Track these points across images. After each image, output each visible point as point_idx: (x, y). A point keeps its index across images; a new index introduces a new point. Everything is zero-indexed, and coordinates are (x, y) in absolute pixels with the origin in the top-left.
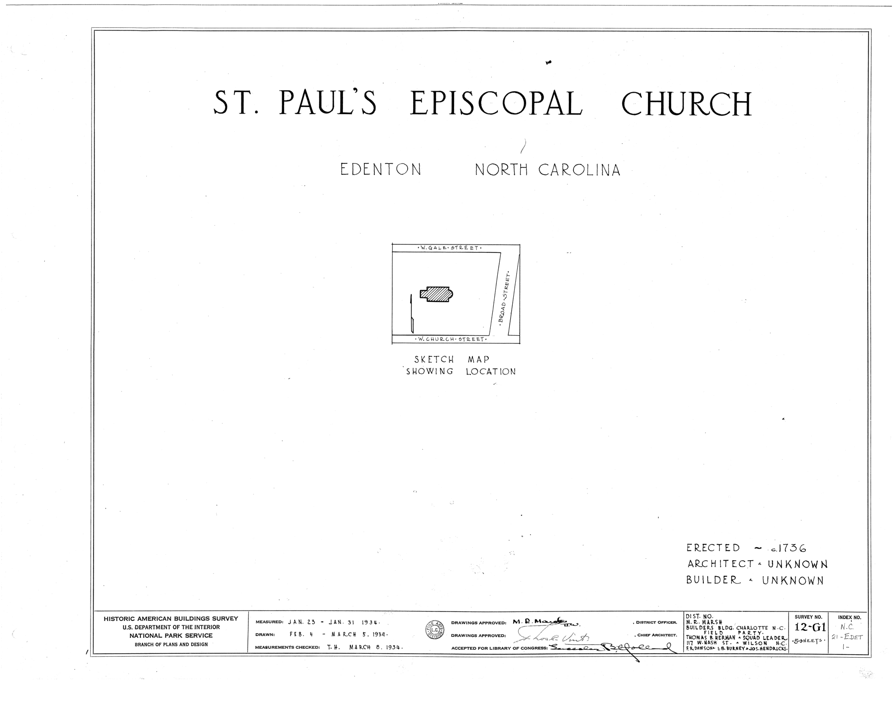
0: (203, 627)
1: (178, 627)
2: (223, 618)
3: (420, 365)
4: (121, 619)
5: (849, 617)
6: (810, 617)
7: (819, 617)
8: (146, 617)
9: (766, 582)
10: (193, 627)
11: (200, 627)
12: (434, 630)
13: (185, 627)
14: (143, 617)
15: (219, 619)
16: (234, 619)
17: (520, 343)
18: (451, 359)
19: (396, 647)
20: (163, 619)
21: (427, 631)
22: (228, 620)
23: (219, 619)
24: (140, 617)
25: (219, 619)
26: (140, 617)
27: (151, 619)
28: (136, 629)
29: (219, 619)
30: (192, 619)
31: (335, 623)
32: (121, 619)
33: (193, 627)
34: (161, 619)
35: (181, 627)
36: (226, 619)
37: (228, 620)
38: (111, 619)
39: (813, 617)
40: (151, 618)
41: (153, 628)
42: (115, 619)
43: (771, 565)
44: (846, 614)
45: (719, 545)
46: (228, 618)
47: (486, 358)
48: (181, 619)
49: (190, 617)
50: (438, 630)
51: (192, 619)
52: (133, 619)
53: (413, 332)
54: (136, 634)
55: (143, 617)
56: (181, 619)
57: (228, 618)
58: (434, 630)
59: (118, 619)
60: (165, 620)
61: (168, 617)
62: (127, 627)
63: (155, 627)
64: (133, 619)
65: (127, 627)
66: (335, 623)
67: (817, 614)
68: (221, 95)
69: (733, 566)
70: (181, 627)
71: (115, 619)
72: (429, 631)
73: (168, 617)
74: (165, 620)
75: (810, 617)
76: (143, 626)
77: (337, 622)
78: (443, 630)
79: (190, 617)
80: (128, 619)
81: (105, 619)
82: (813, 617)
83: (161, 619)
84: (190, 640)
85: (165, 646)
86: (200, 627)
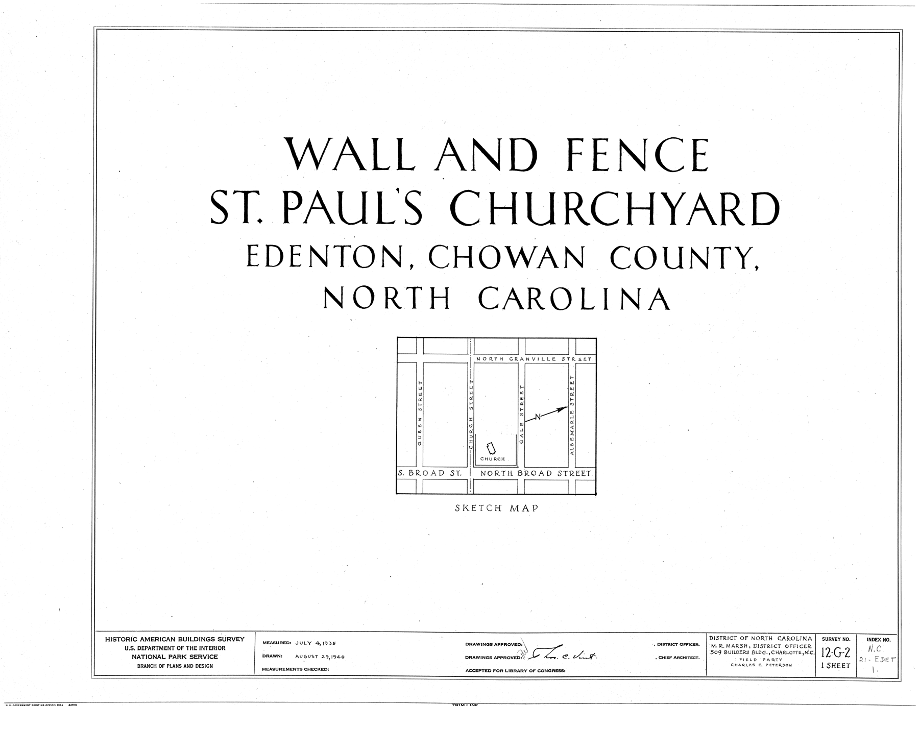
0: (208, 648)
1: (182, 648)
5: (878, 640)
6: (838, 639)
7: (847, 639)
8: (149, 638)
13: (189, 648)
14: (146, 638)
15: (224, 640)
16: (240, 639)
20: (166, 639)
22: (234, 641)
23: (224, 640)
24: (142, 638)
25: (224, 640)
26: (142, 638)
27: (154, 640)
28: (138, 650)
29: (224, 640)
30: (196, 639)
33: (198, 648)
34: (164, 639)
35: (185, 648)
36: (232, 640)
37: (234, 641)
38: (112, 640)
39: (841, 639)
40: (154, 639)
41: (156, 648)
42: (117, 639)
46: (234, 638)
48: (185, 639)
49: (195, 638)
52: (135, 639)
55: (146, 638)
56: (185, 639)
57: (234, 638)
59: (120, 639)
61: (172, 638)
63: (158, 648)
64: (135, 639)
67: (886, 637)
70: (185, 648)
71: (117, 639)
73: (172, 638)
75: (838, 639)
76: (146, 647)
79: (195, 638)
80: (130, 640)
81: (106, 639)
82: (841, 639)
83: (164, 639)
85: (169, 667)
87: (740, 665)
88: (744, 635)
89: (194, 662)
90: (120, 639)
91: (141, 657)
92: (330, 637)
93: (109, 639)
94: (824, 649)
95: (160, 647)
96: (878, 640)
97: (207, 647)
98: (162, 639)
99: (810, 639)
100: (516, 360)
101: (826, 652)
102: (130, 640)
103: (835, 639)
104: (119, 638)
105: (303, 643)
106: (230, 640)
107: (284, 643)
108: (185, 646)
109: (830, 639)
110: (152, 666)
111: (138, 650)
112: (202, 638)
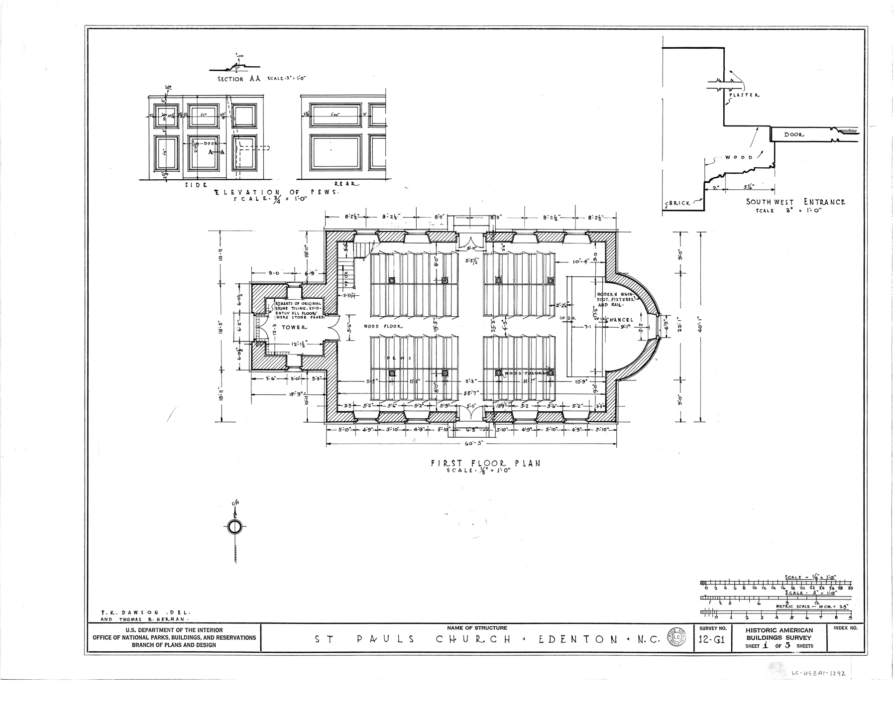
0: (206, 630)
1: (181, 630)
4: (763, 630)
6: (714, 629)
7: (724, 628)
8: (788, 629)
11: (203, 630)
13: (188, 630)
14: (785, 629)
15: (792, 638)
16: (807, 638)
17: (567, 277)
19: (316, 378)
20: (804, 630)
23: (792, 638)
24: (782, 629)
26: (782, 629)
27: (793, 631)
28: (139, 631)
30: (764, 638)
31: (531, 465)
32: (763, 630)
33: (196, 630)
34: (802, 630)
37: (801, 639)
39: (718, 628)
41: (156, 630)
42: (757, 630)
45: (330, 637)
46: (801, 637)
48: (753, 638)
49: (763, 636)
51: (764, 638)
52: (775, 630)
54: (238, 636)
55: (785, 629)
56: (753, 638)
57: (801, 637)
59: (760, 630)
60: (806, 632)
61: (810, 629)
62: (130, 630)
63: (159, 630)
64: (775, 630)
65: (130, 630)
66: (531, 465)
67: (722, 625)
71: (757, 630)
73: (810, 629)
74: (806, 632)
76: (147, 629)
77: (534, 463)
79: (763, 636)
80: (770, 631)
81: (747, 630)
82: (718, 628)
83: (802, 630)
85: (167, 646)
86: (203, 630)
88: (469, 625)
89: (197, 634)
91: (130, 637)
92: (219, 626)
93: (749, 630)
95: (160, 629)
96: (845, 628)
98: (800, 630)
99: (724, 628)
104: (759, 629)
106: (769, 631)
108: (184, 628)
109: (707, 628)
110: (149, 645)
111: (139, 631)
112: (770, 636)
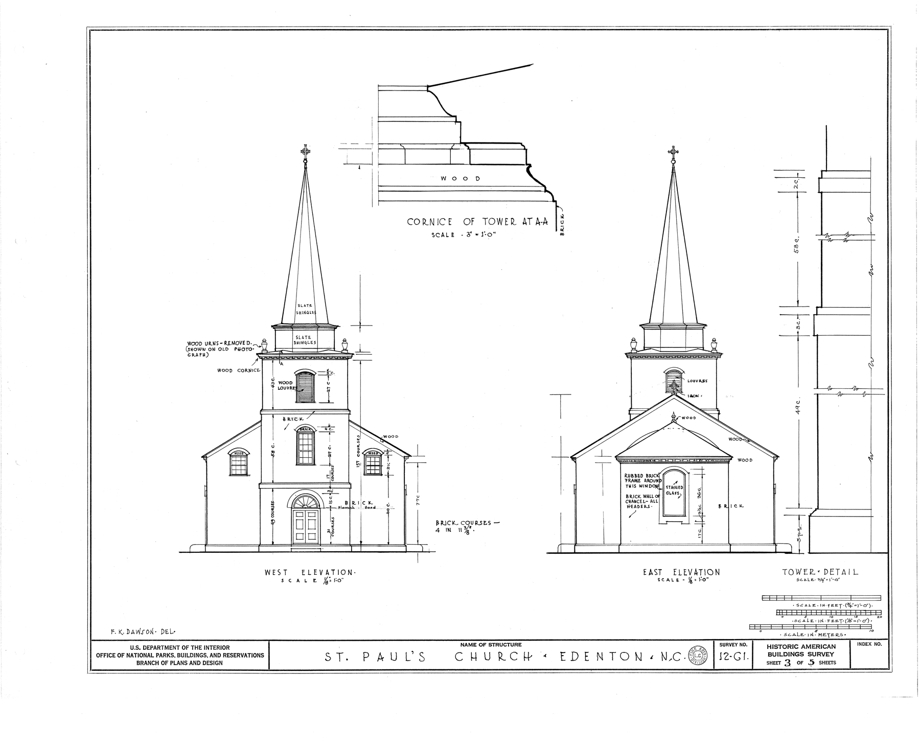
0: (212, 647)
2: (771, 627)
3: (134, 651)
4: (785, 647)
6: (735, 645)
7: (744, 645)
9: (488, 658)
10: (202, 648)
12: (697, 655)
13: (194, 647)
14: (807, 645)
15: (814, 655)
16: (830, 655)
18: (474, 656)
20: (827, 647)
21: (690, 656)
23: (814, 655)
24: (803, 645)
25: (814, 654)
26: (803, 645)
27: (815, 647)
30: (786, 654)
32: (785, 647)
33: (202, 648)
34: (825, 647)
37: (823, 656)
38: (774, 647)
39: (738, 645)
40: (815, 646)
41: (161, 648)
42: (779, 647)
43: (394, 658)
44: (865, 641)
47: (366, 655)
48: (774, 655)
49: (784, 653)
50: (701, 656)
52: (796, 647)
53: (262, 655)
55: (807, 645)
56: (774, 655)
58: (697, 655)
59: (782, 646)
61: (832, 645)
62: (135, 648)
63: (164, 647)
64: (796, 647)
68: (421, 654)
69: (586, 660)
71: (779, 647)
72: (692, 656)
73: (832, 645)
75: (735, 645)
76: (151, 647)
78: (706, 656)
79: (784, 653)
80: (820, 647)
81: (768, 647)
82: (738, 645)
83: (825, 647)
84: (203, 651)
87: (805, 580)
88: (483, 642)
90: (782, 646)
92: (226, 643)
93: (771, 647)
94: (722, 654)
95: (165, 646)
97: (211, 646)
100: (836, 635)
101: (723, 656)
102: (792, 647)
103: (732, 645)
105: (852, 572)
107: (575, 490)
108: (190, 646)
112: (791, 653)
